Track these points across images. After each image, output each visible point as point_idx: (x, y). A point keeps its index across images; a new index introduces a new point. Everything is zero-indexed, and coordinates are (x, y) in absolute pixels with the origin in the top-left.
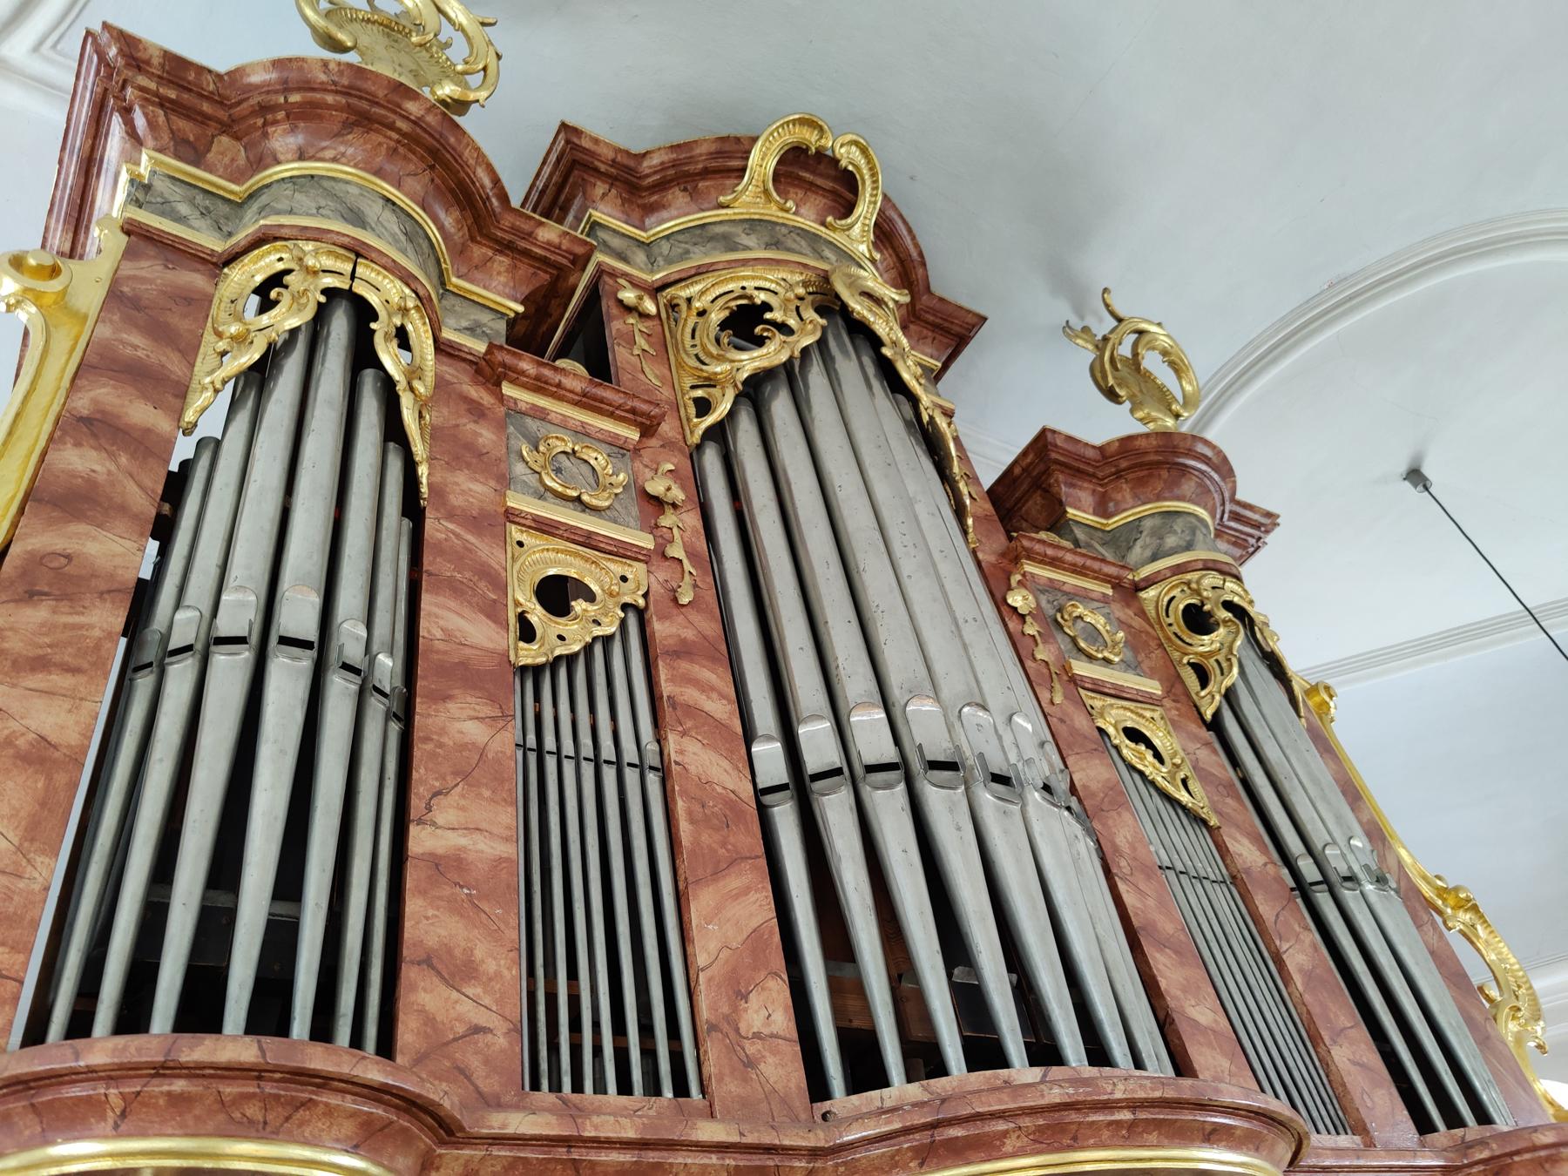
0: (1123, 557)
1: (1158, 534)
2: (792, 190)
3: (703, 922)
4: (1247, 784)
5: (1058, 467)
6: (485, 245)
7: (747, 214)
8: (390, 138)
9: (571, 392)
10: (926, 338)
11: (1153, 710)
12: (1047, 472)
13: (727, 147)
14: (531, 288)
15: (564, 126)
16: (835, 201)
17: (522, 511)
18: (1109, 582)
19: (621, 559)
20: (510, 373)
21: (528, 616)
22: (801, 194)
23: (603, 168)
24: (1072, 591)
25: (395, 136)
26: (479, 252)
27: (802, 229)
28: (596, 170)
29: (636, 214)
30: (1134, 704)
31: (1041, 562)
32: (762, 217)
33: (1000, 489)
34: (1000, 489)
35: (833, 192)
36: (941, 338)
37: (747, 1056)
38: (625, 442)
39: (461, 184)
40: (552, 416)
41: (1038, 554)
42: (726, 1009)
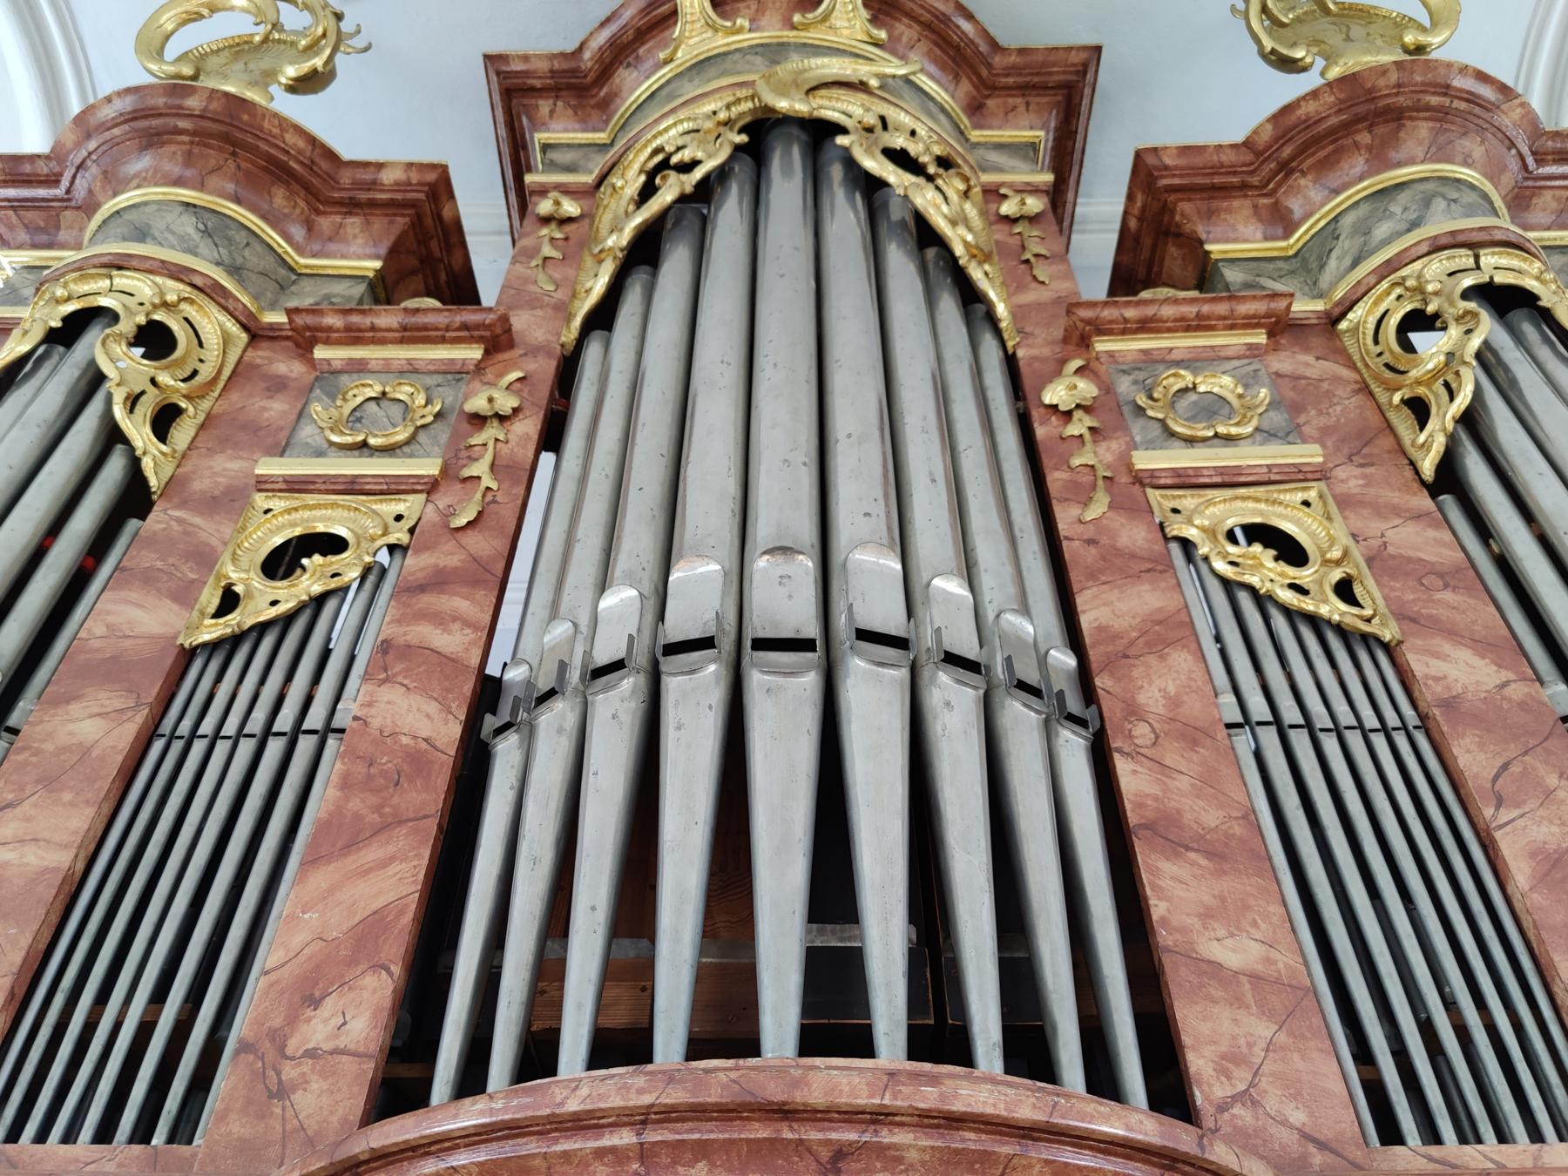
0: (1315, 283)
1: (1364, 229)
4: (1506, 567)
5: (1179, 195)
6: (331, 213)
8: (184, 143)
9: (389, 330)
10: (1014, 108)
11: (1304, 489)
12: (1166, 209)
14: (392, 238)
15: (488, 58)
17: (272, 476)
20: (319, 334)
21: (234, 588)
24: (1190, 356)
25: (186, 138)
26: (325, 223)
28: (533, 89)
31: (1124, 332)
33: (1125, 258)
36: (1037, 99)
37: (280, 1081)
39: (271, 159)
40: (373, 365)
41: (1111, 322)
42: (277, 1021)
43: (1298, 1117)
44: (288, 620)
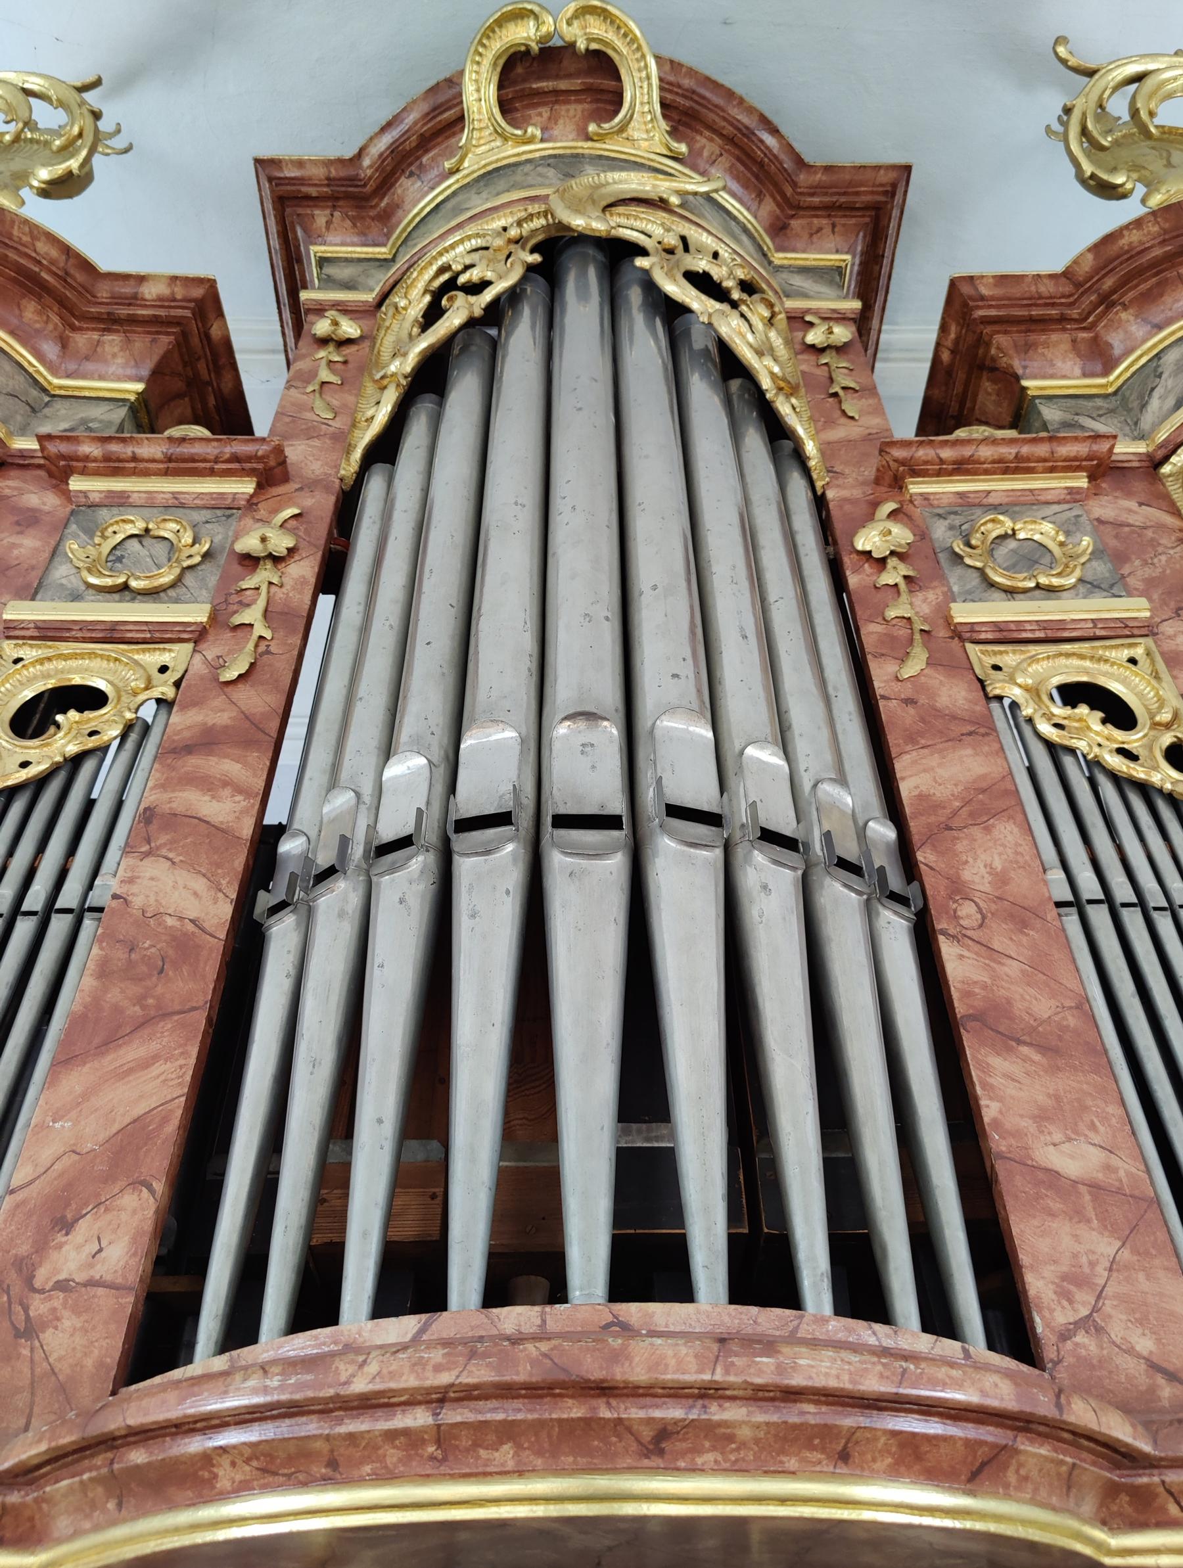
0: (1136, 424)
2: (532, 112)
3: (49, 1119)
5: (996, 328)
6: (88, 329)
7: (479, 169)
9: (154, 461)
10: (819, 230)
11: (1131, 645)
12: (982, 342)
13: (441, 98)
14: (156, 358)
16: (597, 101)
17: (23, 621)
18: (1078, 469)
19: (157, 646)
20: (74, 464)
22: (545, 111)
23: (313, 192)
24: (1006, 500)
26: (81, 340)
27: (555, 156)
28: (308, 197)
29: (375, 228)
30: (1087, 645)
31: (939, 473)
32: (499, 164)
34: (936, 392)
35: (588, 90)
36: (843, 221)
38: (234, 499)
40: (134, 498)
41: (926, 463)
43: (1145, 1345)
44: (41, 782)
